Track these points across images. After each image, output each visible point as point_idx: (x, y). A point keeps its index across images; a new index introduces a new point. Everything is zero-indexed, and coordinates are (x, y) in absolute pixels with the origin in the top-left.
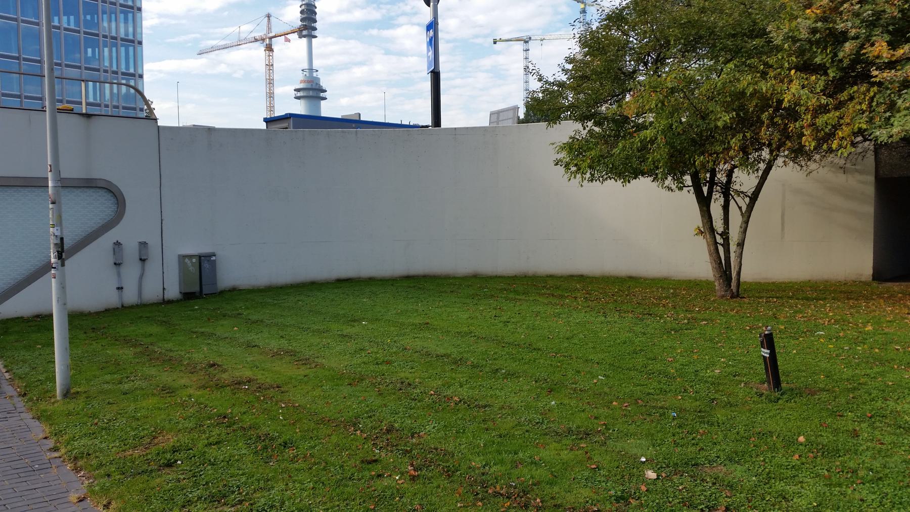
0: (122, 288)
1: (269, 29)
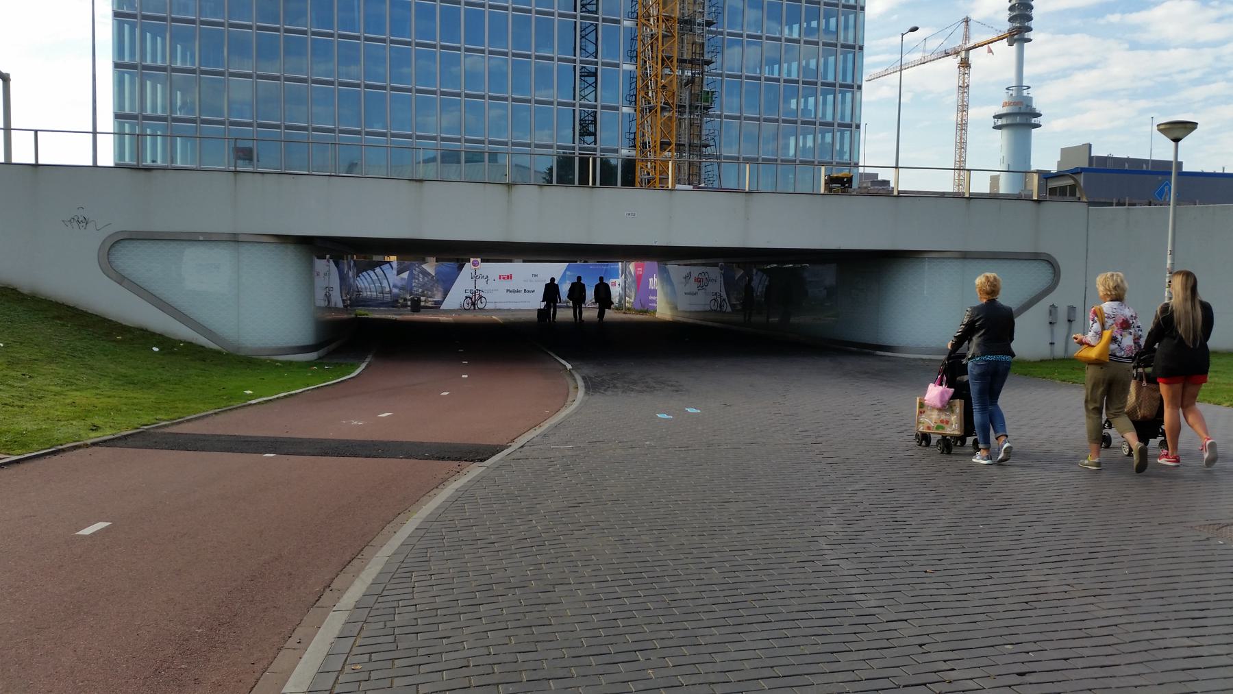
0: (1054, 344)
1: (967, 37)
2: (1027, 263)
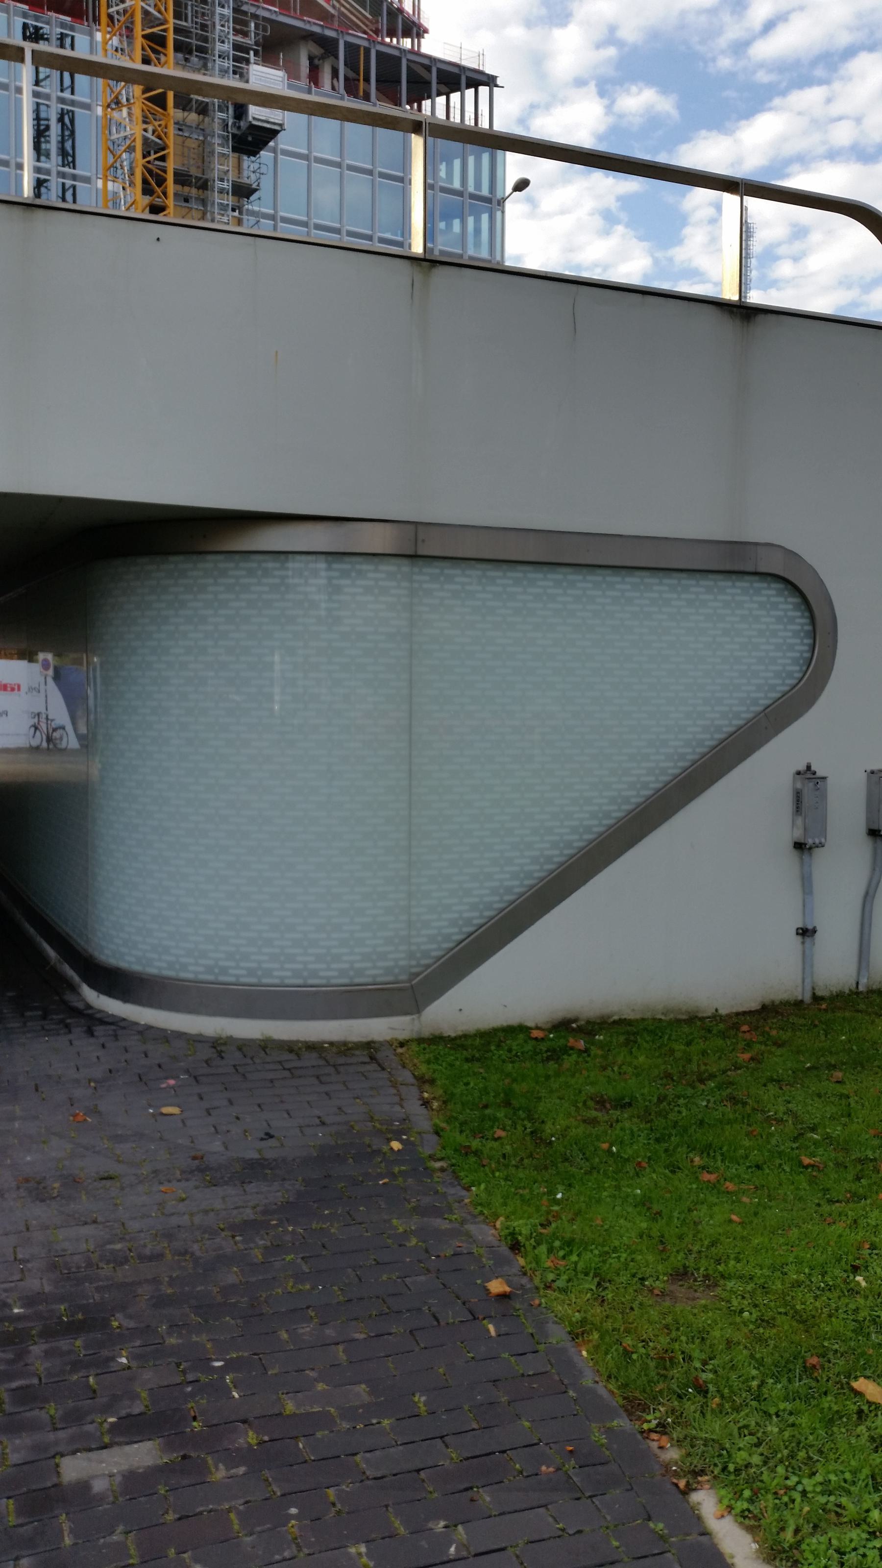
2: (698, 588)
